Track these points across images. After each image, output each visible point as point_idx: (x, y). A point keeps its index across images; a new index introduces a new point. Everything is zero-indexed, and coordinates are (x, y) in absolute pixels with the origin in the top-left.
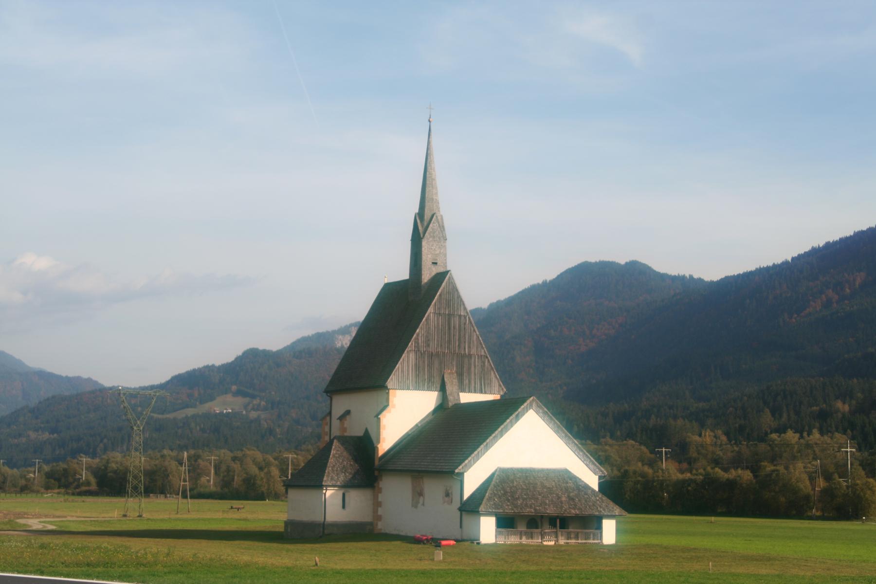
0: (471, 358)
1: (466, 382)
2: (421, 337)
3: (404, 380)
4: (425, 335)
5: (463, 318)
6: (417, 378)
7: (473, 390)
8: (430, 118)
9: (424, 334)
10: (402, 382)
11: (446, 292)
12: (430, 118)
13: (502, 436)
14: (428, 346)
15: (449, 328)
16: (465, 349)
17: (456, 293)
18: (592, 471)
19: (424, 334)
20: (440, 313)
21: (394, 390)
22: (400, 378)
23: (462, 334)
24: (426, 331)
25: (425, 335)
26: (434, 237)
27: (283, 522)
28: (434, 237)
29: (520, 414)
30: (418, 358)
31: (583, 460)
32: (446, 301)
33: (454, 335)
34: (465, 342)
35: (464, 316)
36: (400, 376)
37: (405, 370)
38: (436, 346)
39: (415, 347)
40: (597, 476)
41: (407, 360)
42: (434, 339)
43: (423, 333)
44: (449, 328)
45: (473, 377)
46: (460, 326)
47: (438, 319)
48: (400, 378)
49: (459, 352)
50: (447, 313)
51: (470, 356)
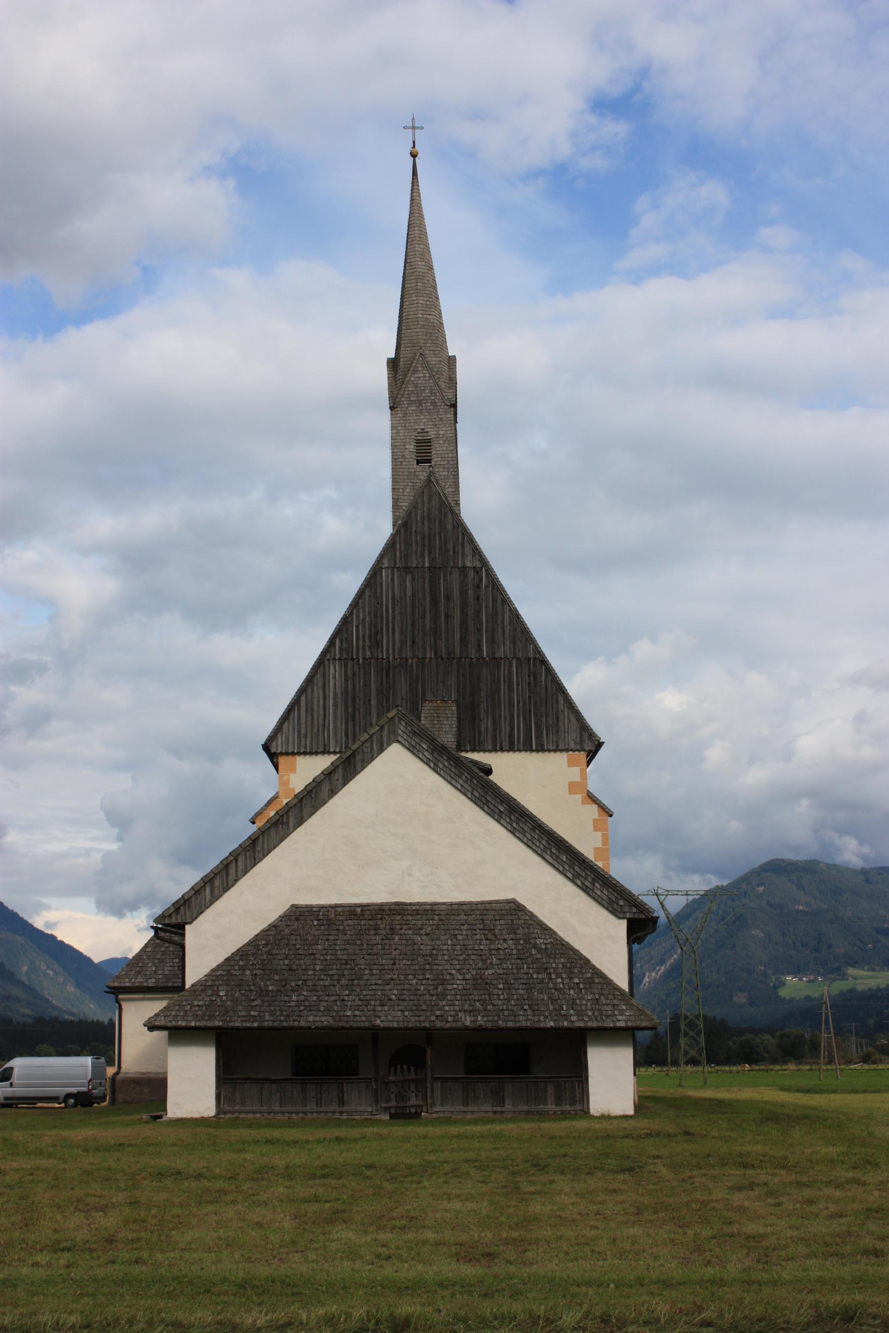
0: (499, 666)
1: (486, 724)
2: (357, 626)
3: (315, 731)
4: (367, 619)
5: (471, 573)
6: (350, 724)
7: (506, 745)
8: (414, 147)
9: (364, 620)
10: (309, 735)
11: (423, 518)
12: (414, 147)
13: (300, 822)
14: (378, 644)
15: (435, 601)
16: (479, 645)
17: (450, 516)
18: (603, 906)
19: (364, 620)
20: (405, 568)
21: (290, 757)
22: (303, 726)
23: (471, 612)
24: (369, 612)
25: (367, 619)
26: (420, 402)
27: (162, 1071)
28: (420, 402)
29: (358, 757)
30: (350, 674)
31: (570, 876)
32: (423, 538)
33: (447, 616)
34: (479, 630)
35: (474, 568)
36: (303, 721)
37: (315, 707)
38: (397, 645)
39: (341, 649)
40: (624, 923)
41: (320, 684)
42: (393, 630)
43: (361, 616)
44: (435, 601)
45: (504, 711)
46: (463, 594)
47: (403, 582)
48: (303, 726)
49: (464, 655)
50: (426, 565)
51: (496, 661)
